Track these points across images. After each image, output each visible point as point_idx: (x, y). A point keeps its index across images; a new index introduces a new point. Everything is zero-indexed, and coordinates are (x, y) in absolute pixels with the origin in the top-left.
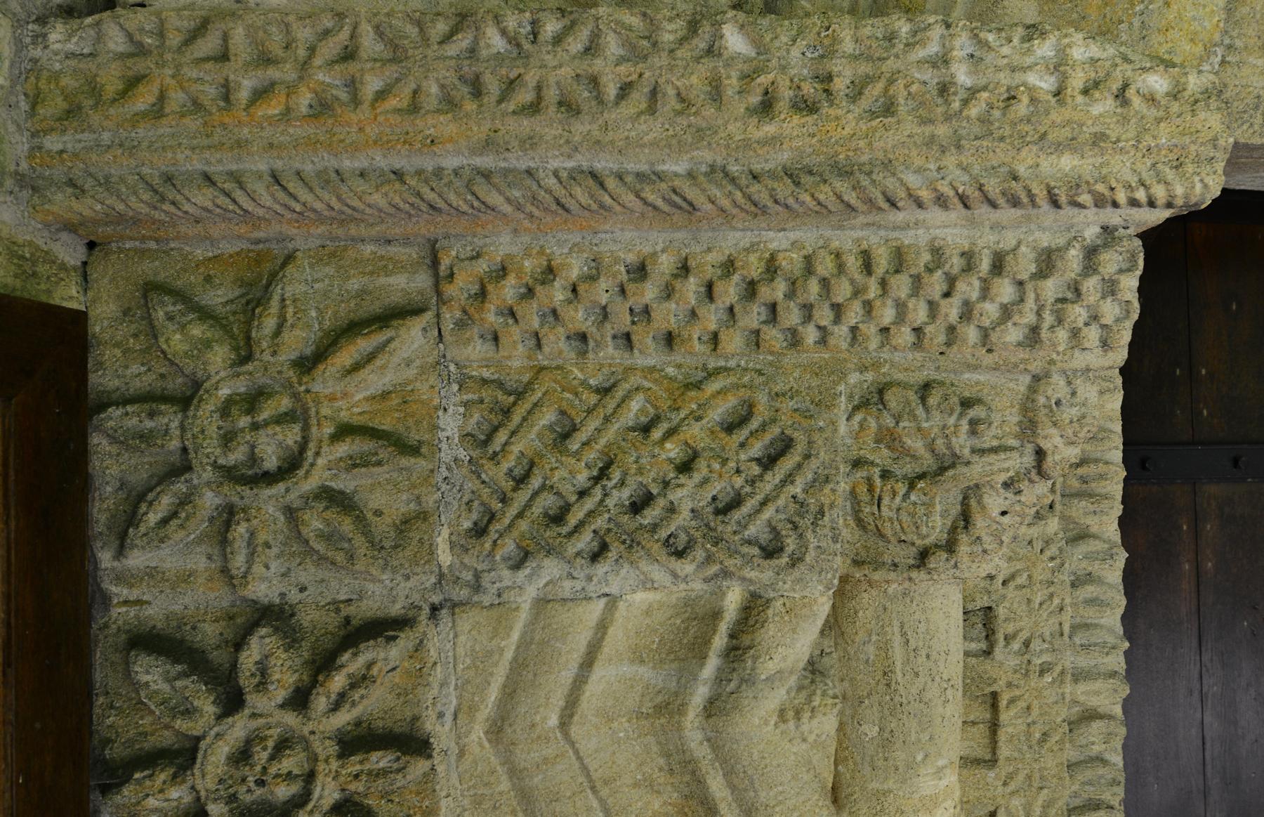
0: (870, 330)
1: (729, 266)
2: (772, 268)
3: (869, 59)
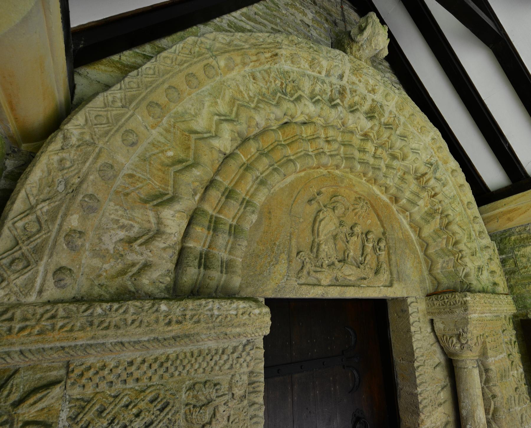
0: (192, 371)
1: (156, 360)
2: (168, 359)
3: (195, 310)
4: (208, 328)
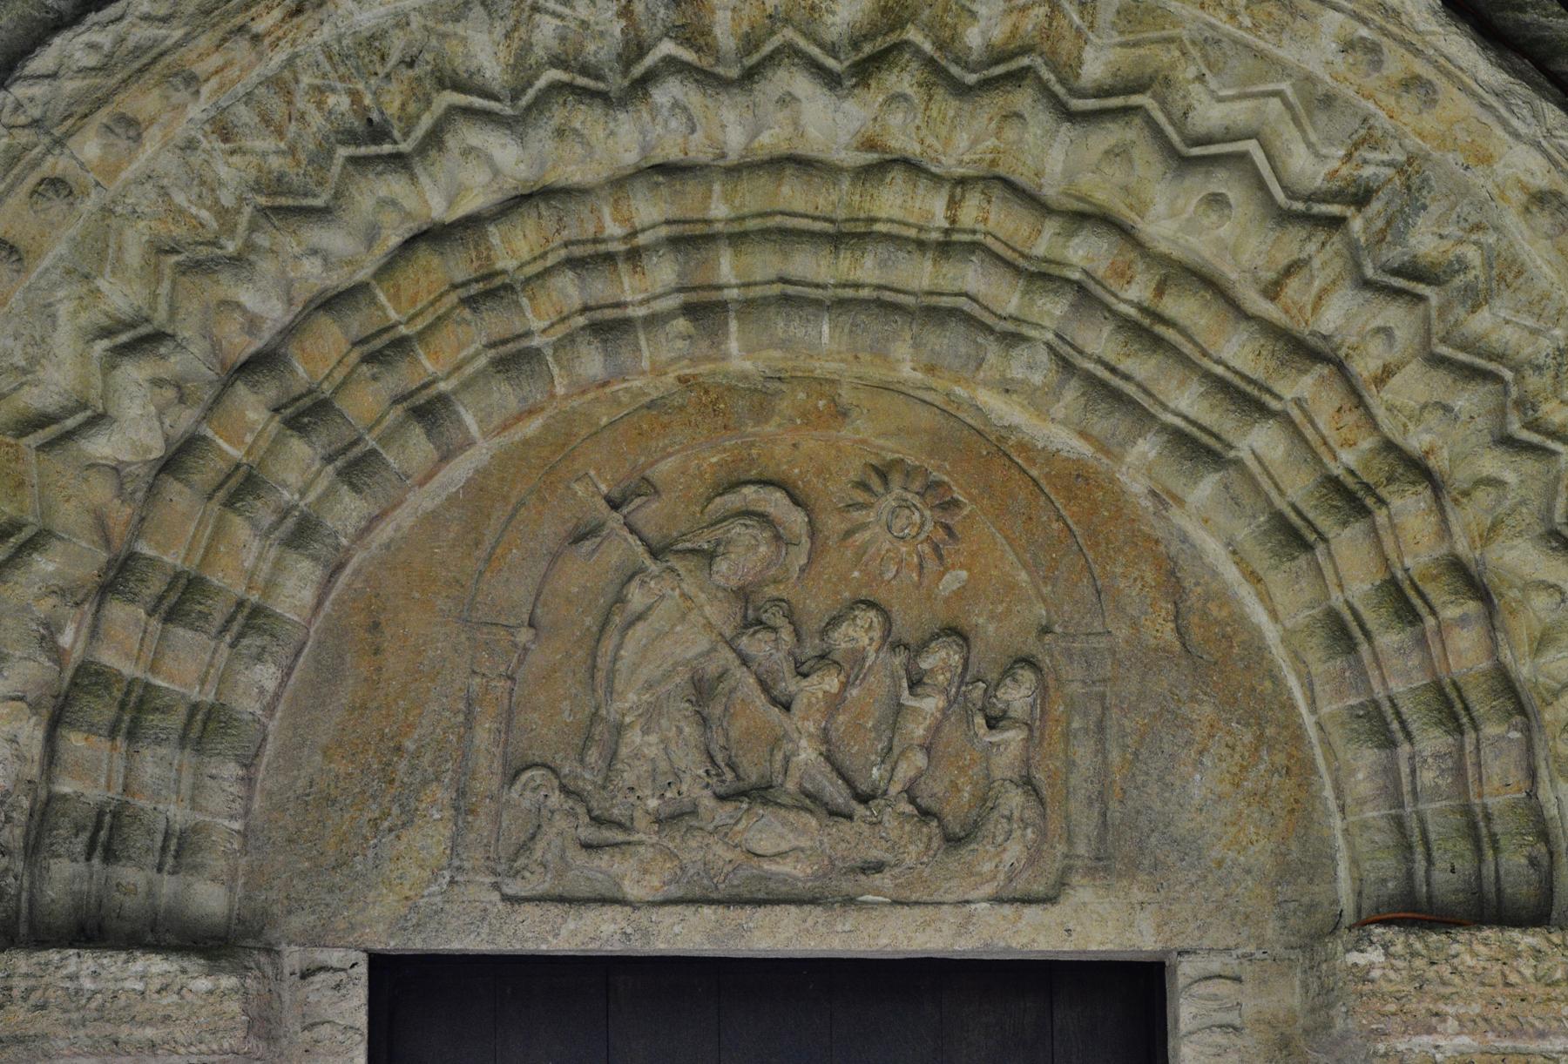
4: (69, 1022)
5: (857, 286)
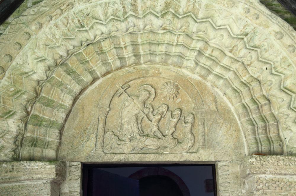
5: (162, 52)
